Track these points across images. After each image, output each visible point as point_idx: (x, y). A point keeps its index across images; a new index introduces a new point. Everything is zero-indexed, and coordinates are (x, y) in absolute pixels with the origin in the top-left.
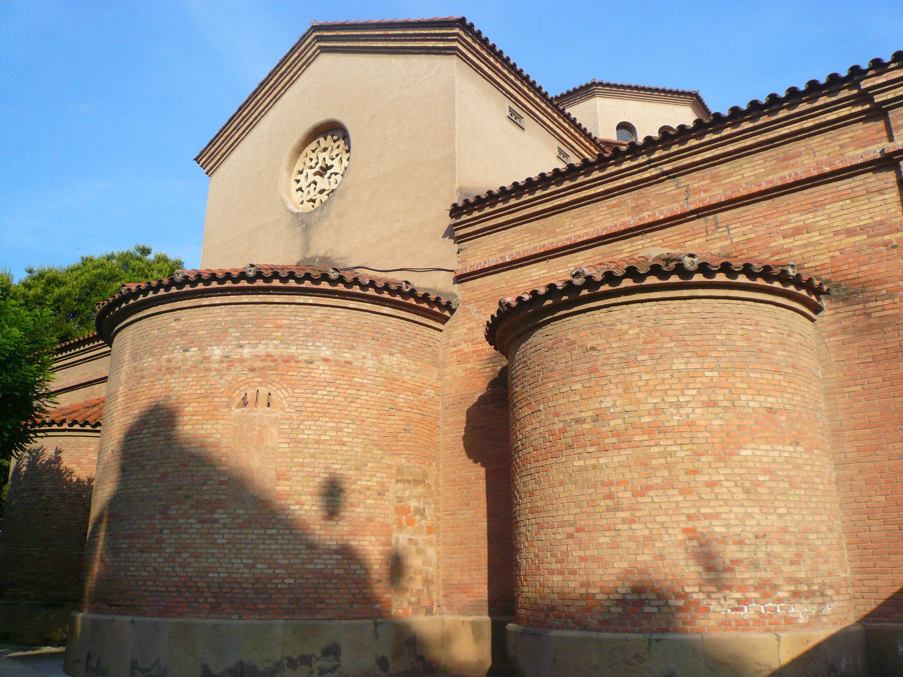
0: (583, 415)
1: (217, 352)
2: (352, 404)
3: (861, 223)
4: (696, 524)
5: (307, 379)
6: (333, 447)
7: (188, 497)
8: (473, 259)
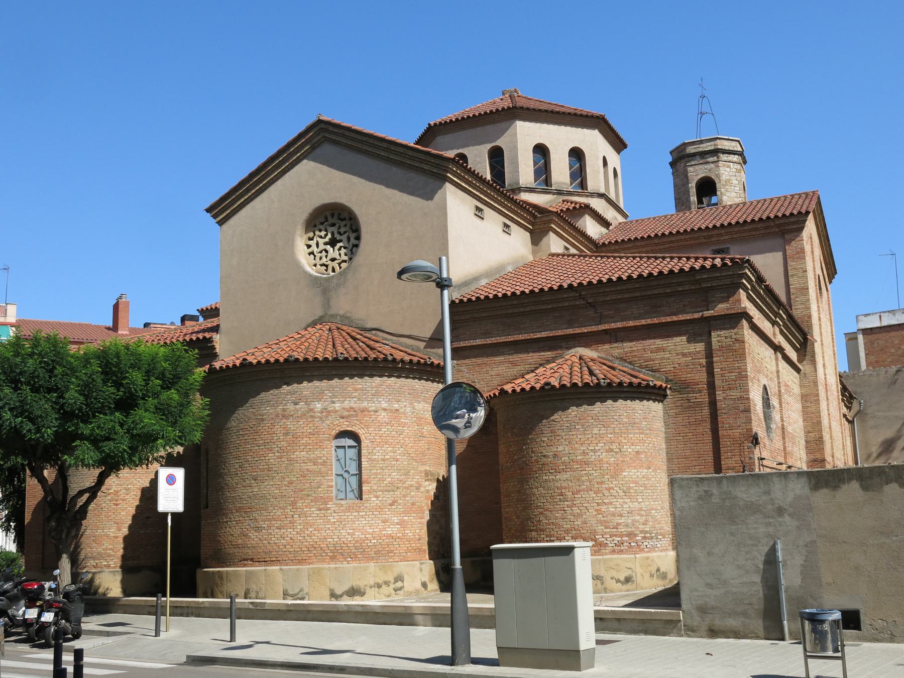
1: (318, 406)
3: (690, 351)
4: (601, 507)
7: (309, 495)
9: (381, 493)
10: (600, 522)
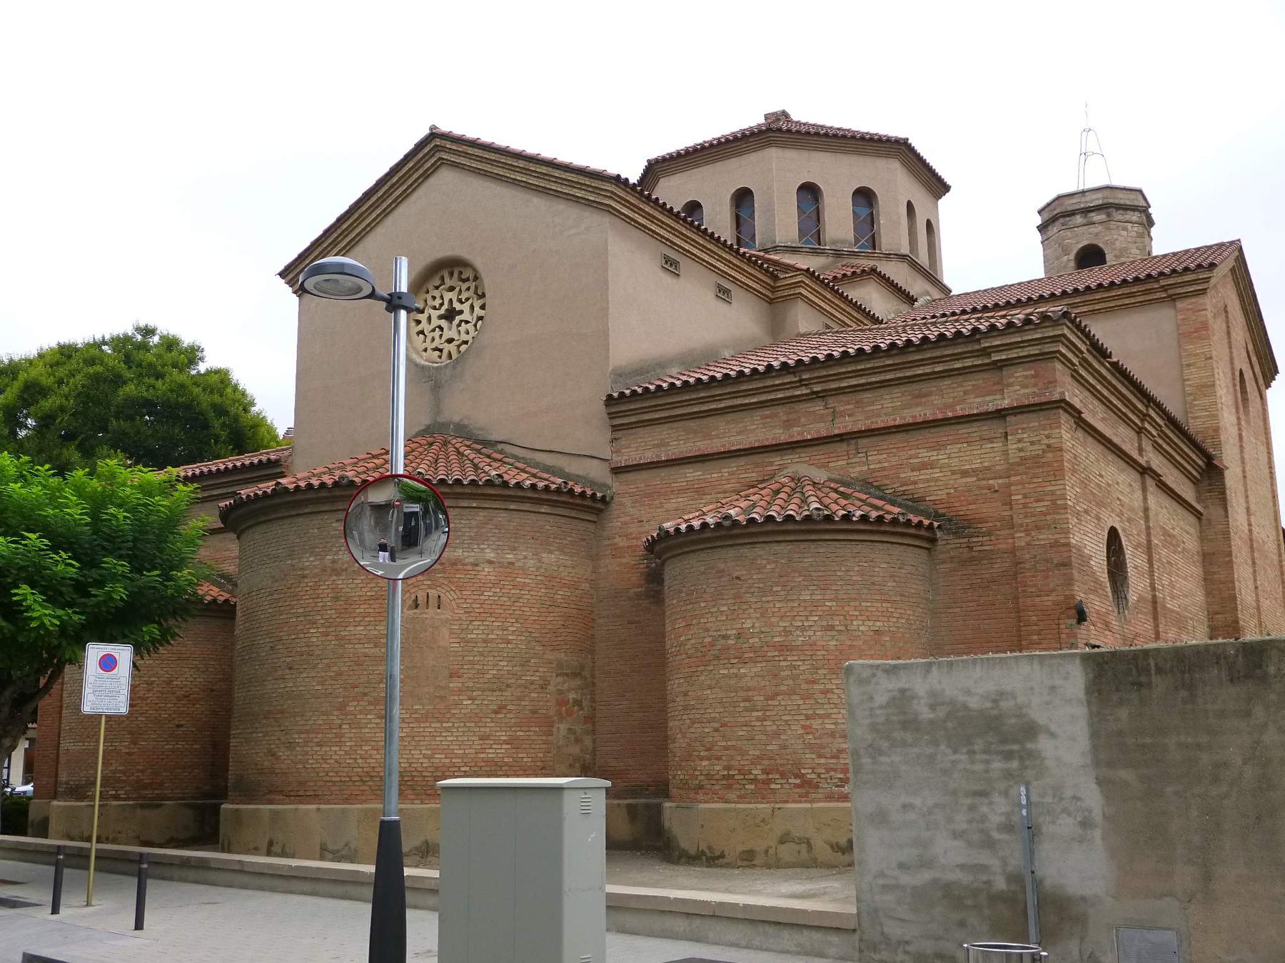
0: (729, 632)
2: (516, 604)
3: (973, 466)
4: (812, 721)
5: (473, 581)
6: (500, 646)
7: (365, 694)
8: (628, 450)
9: (480, 693)
10: (811, 747)
